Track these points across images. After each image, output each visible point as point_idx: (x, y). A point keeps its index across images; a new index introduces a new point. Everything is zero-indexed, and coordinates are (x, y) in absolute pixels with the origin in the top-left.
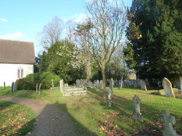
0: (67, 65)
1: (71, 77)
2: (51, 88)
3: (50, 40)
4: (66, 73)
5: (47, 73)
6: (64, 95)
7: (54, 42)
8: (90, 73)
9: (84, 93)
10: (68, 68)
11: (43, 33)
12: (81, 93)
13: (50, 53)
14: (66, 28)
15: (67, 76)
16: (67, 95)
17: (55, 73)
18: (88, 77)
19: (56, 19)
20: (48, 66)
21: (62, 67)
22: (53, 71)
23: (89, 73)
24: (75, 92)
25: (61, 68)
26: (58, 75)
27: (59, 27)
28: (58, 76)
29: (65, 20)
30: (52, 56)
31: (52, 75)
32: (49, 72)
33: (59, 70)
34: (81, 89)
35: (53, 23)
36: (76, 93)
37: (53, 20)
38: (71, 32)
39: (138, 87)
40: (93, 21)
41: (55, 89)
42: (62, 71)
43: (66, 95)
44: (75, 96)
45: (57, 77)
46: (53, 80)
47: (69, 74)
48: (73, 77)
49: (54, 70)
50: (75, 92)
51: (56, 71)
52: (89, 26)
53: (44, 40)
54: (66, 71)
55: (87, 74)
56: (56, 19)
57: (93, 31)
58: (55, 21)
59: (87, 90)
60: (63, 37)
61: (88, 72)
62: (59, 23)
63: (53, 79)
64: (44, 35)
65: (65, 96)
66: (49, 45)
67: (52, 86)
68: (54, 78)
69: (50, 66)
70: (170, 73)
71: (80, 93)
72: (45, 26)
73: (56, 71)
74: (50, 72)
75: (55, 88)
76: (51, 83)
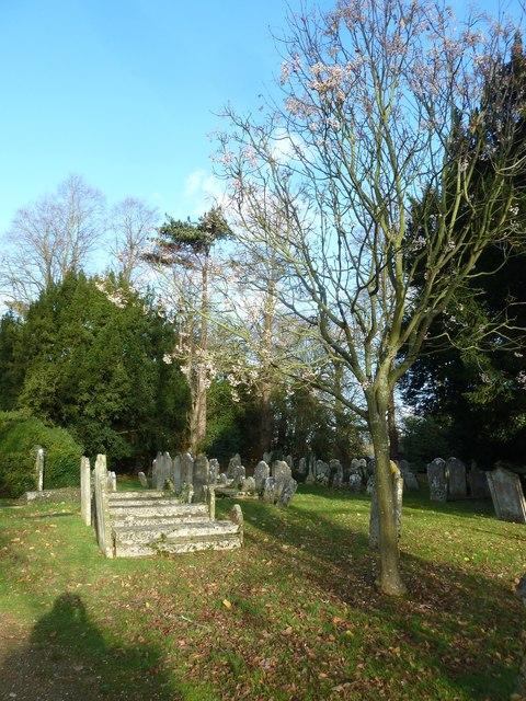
0: (112, 385)
1: (127, 438)
2: (31, 496)
3: (38, 274)
4: (104, 417)
5: (13, 415)
6: (110, 555)
7: (59, 278)
8: (203, 424)
9: (228, 537)
10: (117, 395)
11: (11, 237)
12: (211, 538)
13: (39, 321)
14: (113, 227)
15: (108, 432)
16: (132, 550)
17: (52, 417)
18: (194, 440)
19: (75, 188)
20: (20, 382)
21: (91, 390)
22: (44, 406)
23: (198, 422)
24: (175, 534)
25: (86, 396)
26: (64, 425)
27: (85, 224)
28: (65, 432)
29: (114, 198)
30: (45, 333)
31: (39, 425)
32: (22, 411)
33: (75, 403)
34: (202, 508)
35: (60, 200)
36: (183, 540)
37: (62, 191)
38: (132, 248)
39: (448, 501)
40: (230, 217)
41: (52, 500)
42: (89, 410)
43: (121, 553)
44: (178, 557)
45: (64, 440)
46: (41, 451)
47: (117, 424)
48: (142, 437)
49: (50, 400)
50: (175, 534)
51: (58, 409)
52: (215, 227)
53: (14, 268)
54: (107, 412)
55: (193, 426)
56: (75, 188)
57: (222, 249)
58: (69, 194)
59: (241, 519)
60: (98, 263)
61: (195, 417)
62: (87, 203)
63: (43, 446)
64: (13, 249)
65: (118, 563)
66: (33, 294)
67: (33, 487)
68: (50, 442)
69: (30, 384)
70: (503, 435)
71: (203, 539)
72: (21, 212)
73: (57, 408)
74: (26, 412)
75: (49, 493)
76: (30, 468)
